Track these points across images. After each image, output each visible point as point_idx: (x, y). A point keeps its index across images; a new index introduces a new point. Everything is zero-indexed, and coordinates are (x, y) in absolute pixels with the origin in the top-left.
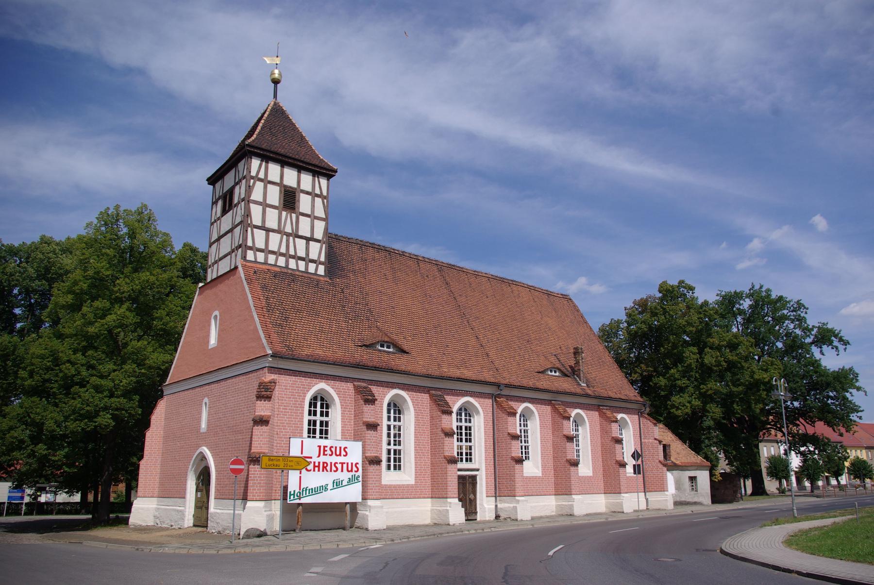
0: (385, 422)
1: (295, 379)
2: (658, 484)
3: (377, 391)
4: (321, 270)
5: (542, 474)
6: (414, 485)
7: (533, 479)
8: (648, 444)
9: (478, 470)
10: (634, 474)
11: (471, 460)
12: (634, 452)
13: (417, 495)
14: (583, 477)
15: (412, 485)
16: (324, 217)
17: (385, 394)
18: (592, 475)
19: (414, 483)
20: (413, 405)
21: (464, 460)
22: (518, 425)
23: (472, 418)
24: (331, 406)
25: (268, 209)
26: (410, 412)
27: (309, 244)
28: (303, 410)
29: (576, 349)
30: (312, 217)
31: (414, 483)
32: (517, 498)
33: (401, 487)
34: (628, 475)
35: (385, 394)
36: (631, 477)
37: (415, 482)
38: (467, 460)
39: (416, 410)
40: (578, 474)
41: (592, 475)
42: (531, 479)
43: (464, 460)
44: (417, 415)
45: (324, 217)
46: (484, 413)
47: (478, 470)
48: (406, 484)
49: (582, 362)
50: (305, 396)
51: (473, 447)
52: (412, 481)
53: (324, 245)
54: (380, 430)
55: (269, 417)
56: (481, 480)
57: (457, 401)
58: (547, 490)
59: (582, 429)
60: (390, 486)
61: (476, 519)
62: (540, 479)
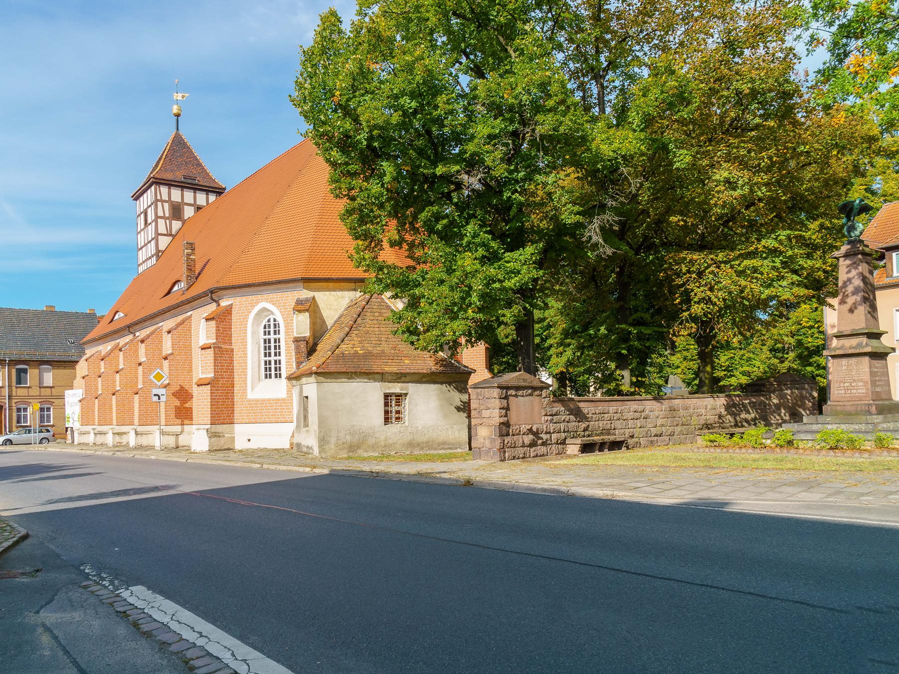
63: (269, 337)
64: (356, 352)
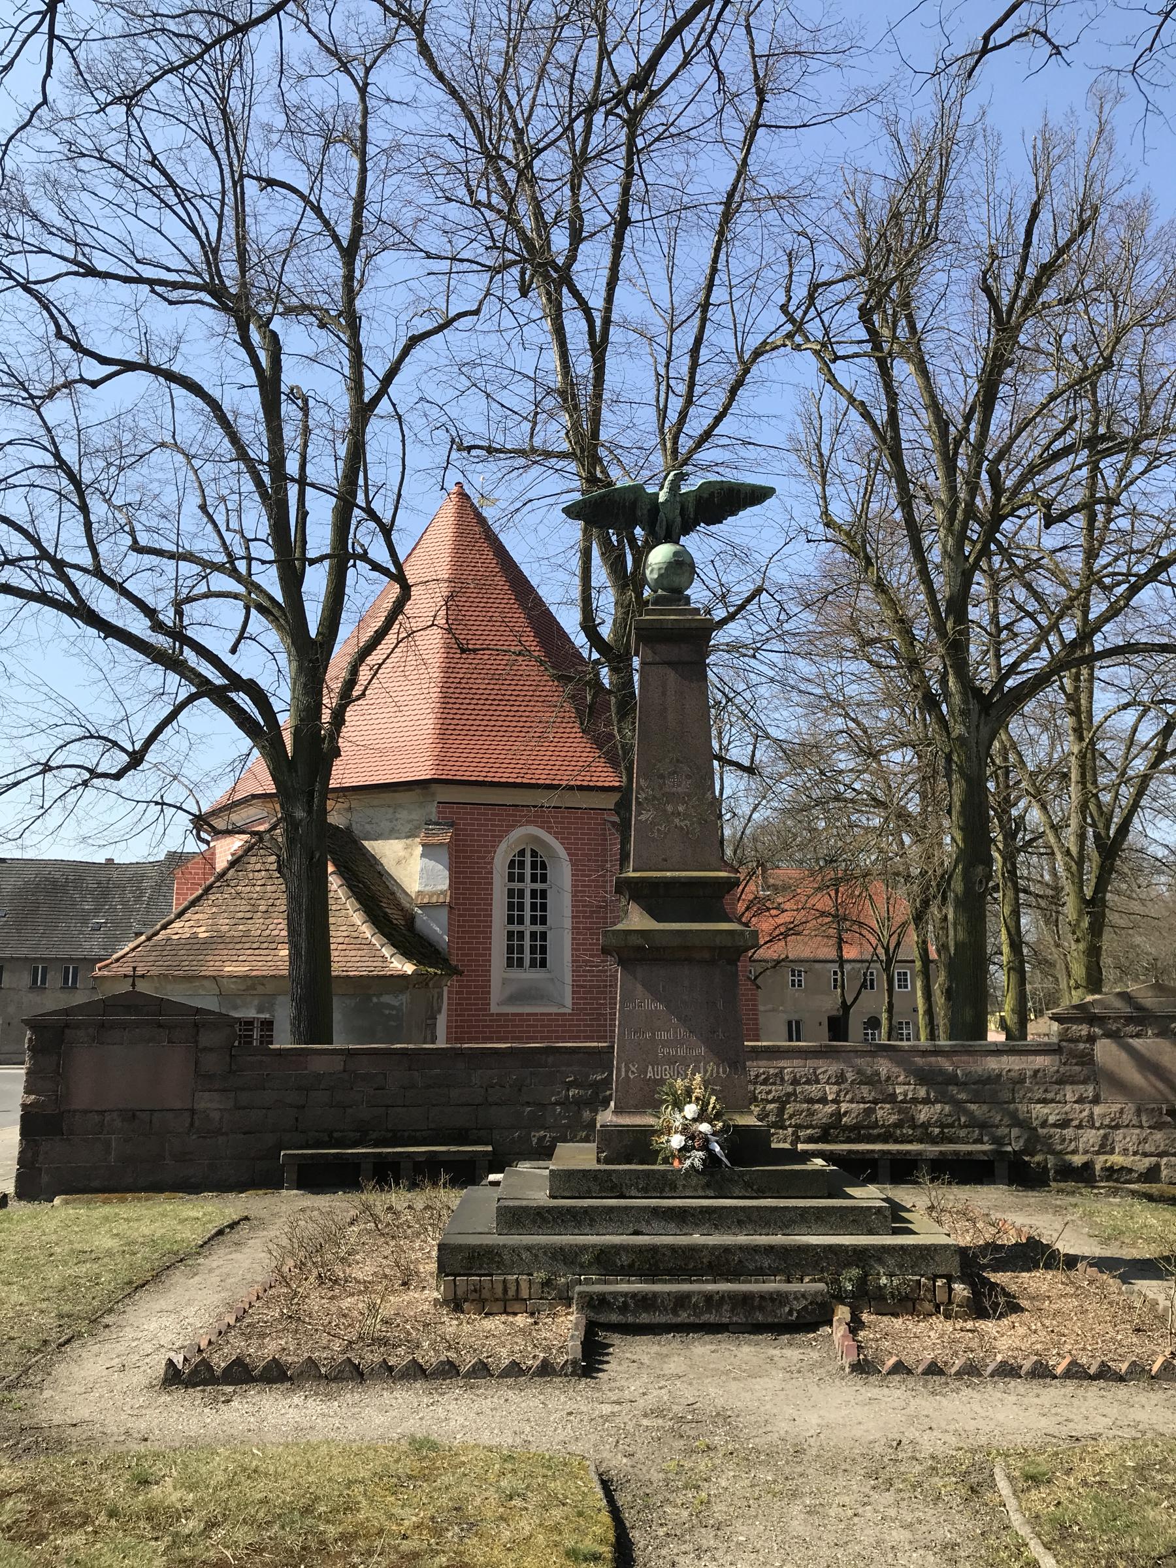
64: (195, 936)
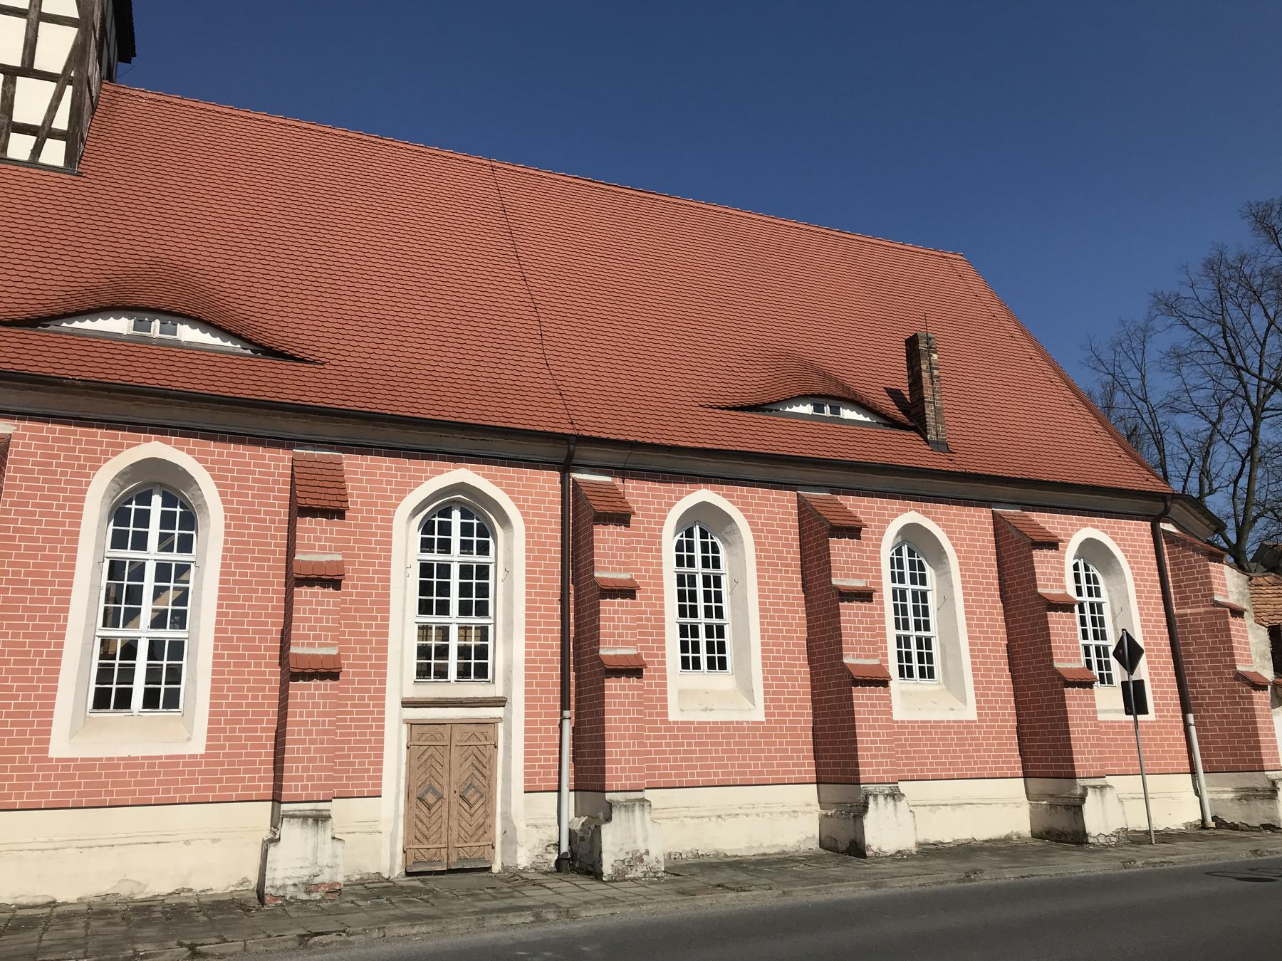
0: (887, 586)
1: (1109, 522)
2: (1238, 748)
3: (639, 495)
4: (54, 153)
5: (767, 715)
6: (202, 756)
7: (728, 729)
8: (1195, 620)
9: (500, 702)
10: (1127, 713)
11: (482, 672)
12: (1121, 640)
13: (213, 789)
14: (903, 725)
15: (194, 756)
16: (77, 16)
17: (98, 460)
18: (975, 718)
19: (203, 751)
20: (221, 494)
21: (916, 672)
22: (669, 555)
23: (490, 540)
24: (1238, 577)
25: (43, 26)
26: (512, 531)
27: (14, 83)
28: (879, 571)
29: (912, 343)
30: (33, 15)
31: (203, 751)
32: (1266, 773)
33: (142, 766)
34: (1101, 717)
35: (98, 460)
36: (1111, 725)
37: (208, 747)
38: (463, 673)
39: (231, 502)
40: (666, 714)
41: (975, 718)
42: (720, 729)
43: (916, 672)
44: (236, 527)
45: (77, 16)
46: (957, 551)
47: (500, 702)
48: (163, 753)
49: (932, 377)
50: (665, 517)
51: (491, 629)
52: (197, 746)
53: (69, 89)
54: (878, 603)
55: (340, 564)
56: (508, 735)
57: (417, 485)
58: (1058, 760)
59: (938, 576)
60: (85, 765)
61: (489, 869)
62: (758, 729)
63: (138, 555)
